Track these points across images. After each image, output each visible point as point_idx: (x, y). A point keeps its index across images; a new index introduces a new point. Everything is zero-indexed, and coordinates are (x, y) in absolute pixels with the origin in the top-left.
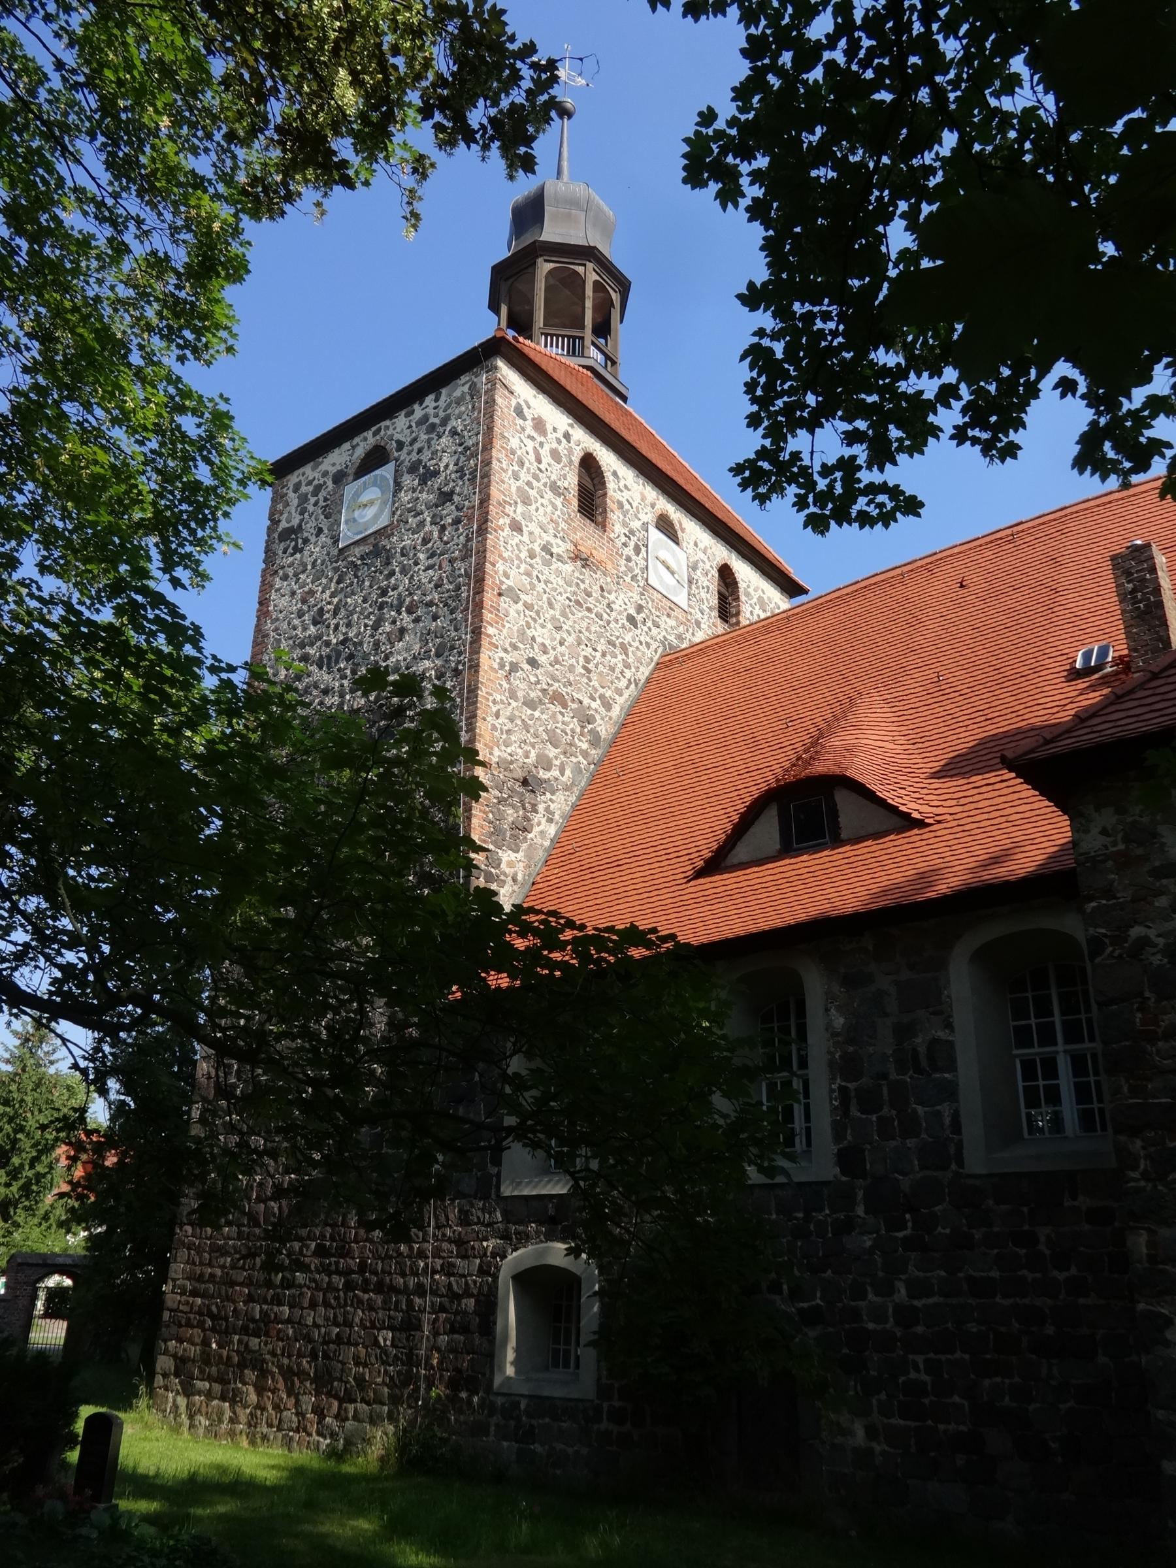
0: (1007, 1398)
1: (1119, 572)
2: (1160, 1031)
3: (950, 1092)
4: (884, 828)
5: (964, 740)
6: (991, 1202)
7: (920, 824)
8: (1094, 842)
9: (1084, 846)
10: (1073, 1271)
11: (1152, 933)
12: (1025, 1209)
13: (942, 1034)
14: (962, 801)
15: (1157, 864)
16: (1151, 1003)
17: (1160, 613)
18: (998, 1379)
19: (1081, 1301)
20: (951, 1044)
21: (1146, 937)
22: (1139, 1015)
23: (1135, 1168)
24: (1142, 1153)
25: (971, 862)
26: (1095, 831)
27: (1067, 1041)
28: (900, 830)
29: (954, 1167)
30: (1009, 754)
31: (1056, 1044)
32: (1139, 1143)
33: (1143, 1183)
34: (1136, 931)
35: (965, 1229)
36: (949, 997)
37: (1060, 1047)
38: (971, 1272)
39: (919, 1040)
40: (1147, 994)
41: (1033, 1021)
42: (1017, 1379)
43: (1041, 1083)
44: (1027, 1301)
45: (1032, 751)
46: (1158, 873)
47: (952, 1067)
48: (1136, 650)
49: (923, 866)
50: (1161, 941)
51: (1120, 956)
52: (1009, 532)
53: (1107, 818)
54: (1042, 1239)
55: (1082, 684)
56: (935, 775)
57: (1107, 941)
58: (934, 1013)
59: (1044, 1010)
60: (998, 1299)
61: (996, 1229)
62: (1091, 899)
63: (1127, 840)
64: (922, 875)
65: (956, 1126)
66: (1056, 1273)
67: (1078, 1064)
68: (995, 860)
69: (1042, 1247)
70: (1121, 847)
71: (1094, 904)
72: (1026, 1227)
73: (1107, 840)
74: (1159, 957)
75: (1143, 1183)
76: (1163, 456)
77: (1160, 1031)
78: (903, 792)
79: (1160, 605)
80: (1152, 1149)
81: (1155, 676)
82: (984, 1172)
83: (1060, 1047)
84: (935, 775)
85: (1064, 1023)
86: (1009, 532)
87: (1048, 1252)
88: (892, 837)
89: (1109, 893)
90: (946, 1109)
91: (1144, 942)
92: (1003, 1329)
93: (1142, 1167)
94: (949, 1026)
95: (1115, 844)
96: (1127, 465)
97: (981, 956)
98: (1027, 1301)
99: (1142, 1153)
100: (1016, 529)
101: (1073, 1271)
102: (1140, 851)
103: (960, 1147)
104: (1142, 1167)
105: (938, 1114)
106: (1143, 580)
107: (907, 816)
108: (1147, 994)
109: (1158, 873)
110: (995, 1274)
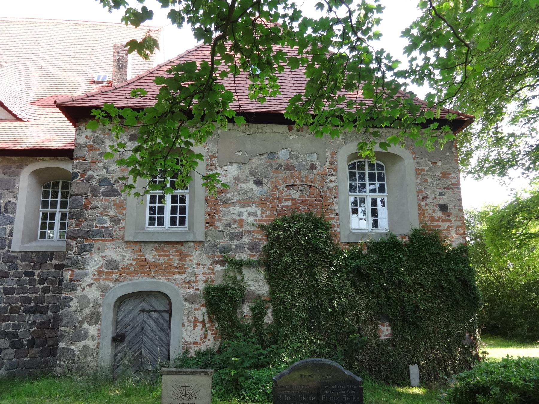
0: (11, 329)
1: (116, 51)
2: (90, 207)
3: (11, 222)
4: (5, 118)
5: (48, 93)
6: (19, 261)
7: (20, 120)
8: (82, 140)
9: (78, 141)
10: (45, 285)
11: (95, 174)
12: (32, 264)
13: (12, 200)
14: (40, 116)
15: (102, 152)
16: (89, 197)
17: (125, 70)
18: (9, 322)
19: (46, 295)
20: (15, 204)
21: (93, 175)
22: (84, 200)
23: (71, 250)
24: (75, 246)
25: (38, 139)
26: (84, 136)
27: (61, 208)
28: (11, 121)
29: (7, 248)
30: (58, 101)
31: (56, 208)
32: (75, 242)
33: (73, 255)
34: (90, 173)
35: (7, 271)
36: (18, 187)
37: (58, 209)
38: (6, 286)
39: (2, 201)
40: (89, 194)
41: (50, 200)
42: (16, 322)
43: (48, 221)
44: (25, 295)
45: (66, 102)
46: (101, 155)
47: (14, 212)
48: (115, 80)
49: (18, 136)
50: (97, 177)
51: (83, 180)
52: (82, 23)
53: (89, 133)
54: (36, 274)
55: (94, 86)
56: (32, 103)
57: (79, 174)
58: (10, 192)
59: (55, 196)
60: (14, 295)
61: (19, 271)
62: (77, 159)
63: (94, 141)
64: (16, 140)
65: (11, 234)
66: (39, 286)
67: (63, 216)
68: (47, 140)
69: (36, 277)
70: (91, 143)
71: (77, 161)
72: (31, 270)
73: (87, 140)
74: (95, 182)
75: (73, 255)
76: (125, 7)
77: (90, 207)
78: (26, 108)
79: (126, 67)
80: (79, 245)
81: (116, 89)
82: (18, 251)
83: (58, 209)
84: (32, 103)
85: (61, 202)
86: (82, 23)
87: (37, 279)
88: (7, 122)
89: (83, 158)
90: (8, 228)
91: (91, 177)
92: (14, 305)
93: (74, 250)
94: (16, 197)
95: (89, 142)
96: (112, 4)
97: (36, 173)
98: (25, 295)
99: (75, 246)
100: (85, 23)
101: (45, 285)
102: (97, 146)
103: (11, 241)
104: (74, 250)
105: (5, 229)
106: (122, 57)
107: (15, 116)
108: (89, 194)
109: (101, 155)
110: (15, 286)
